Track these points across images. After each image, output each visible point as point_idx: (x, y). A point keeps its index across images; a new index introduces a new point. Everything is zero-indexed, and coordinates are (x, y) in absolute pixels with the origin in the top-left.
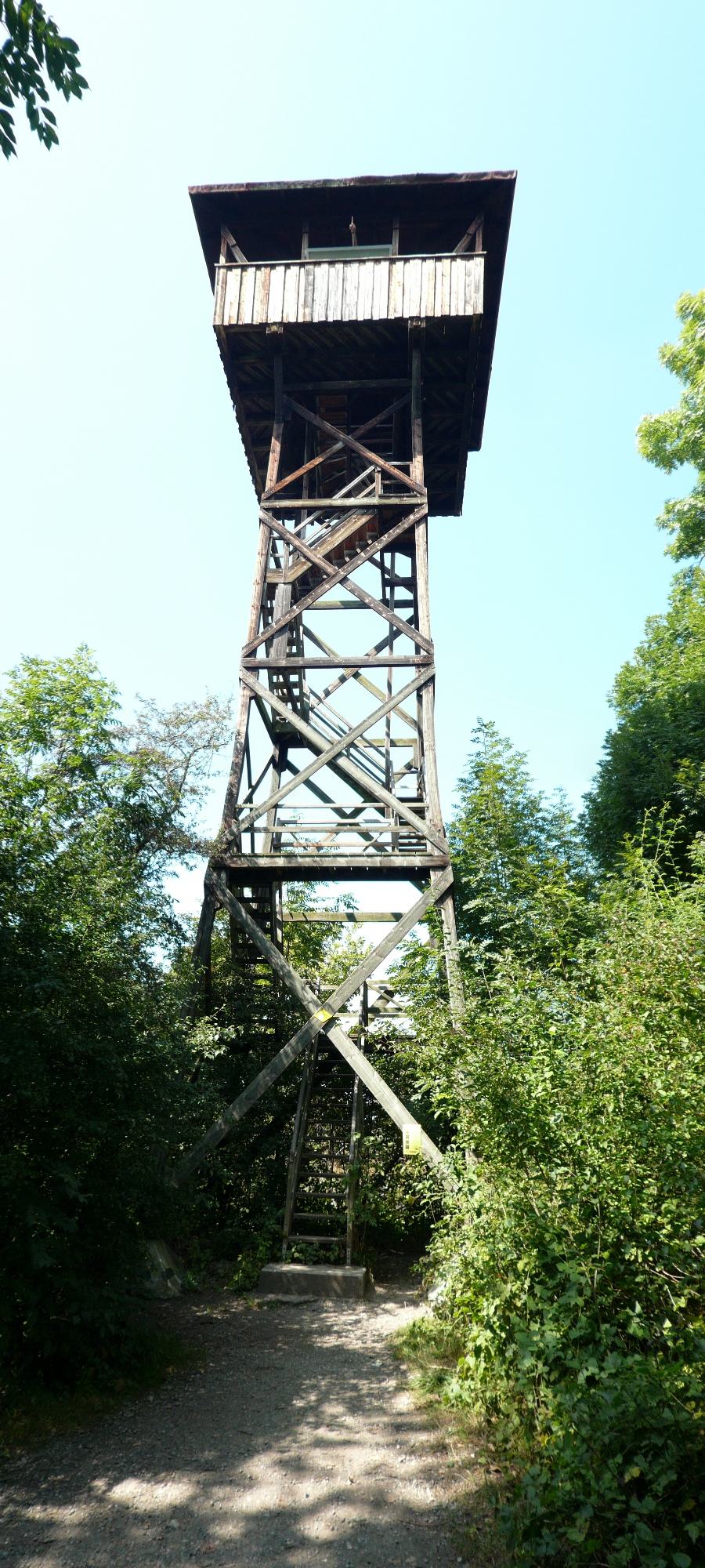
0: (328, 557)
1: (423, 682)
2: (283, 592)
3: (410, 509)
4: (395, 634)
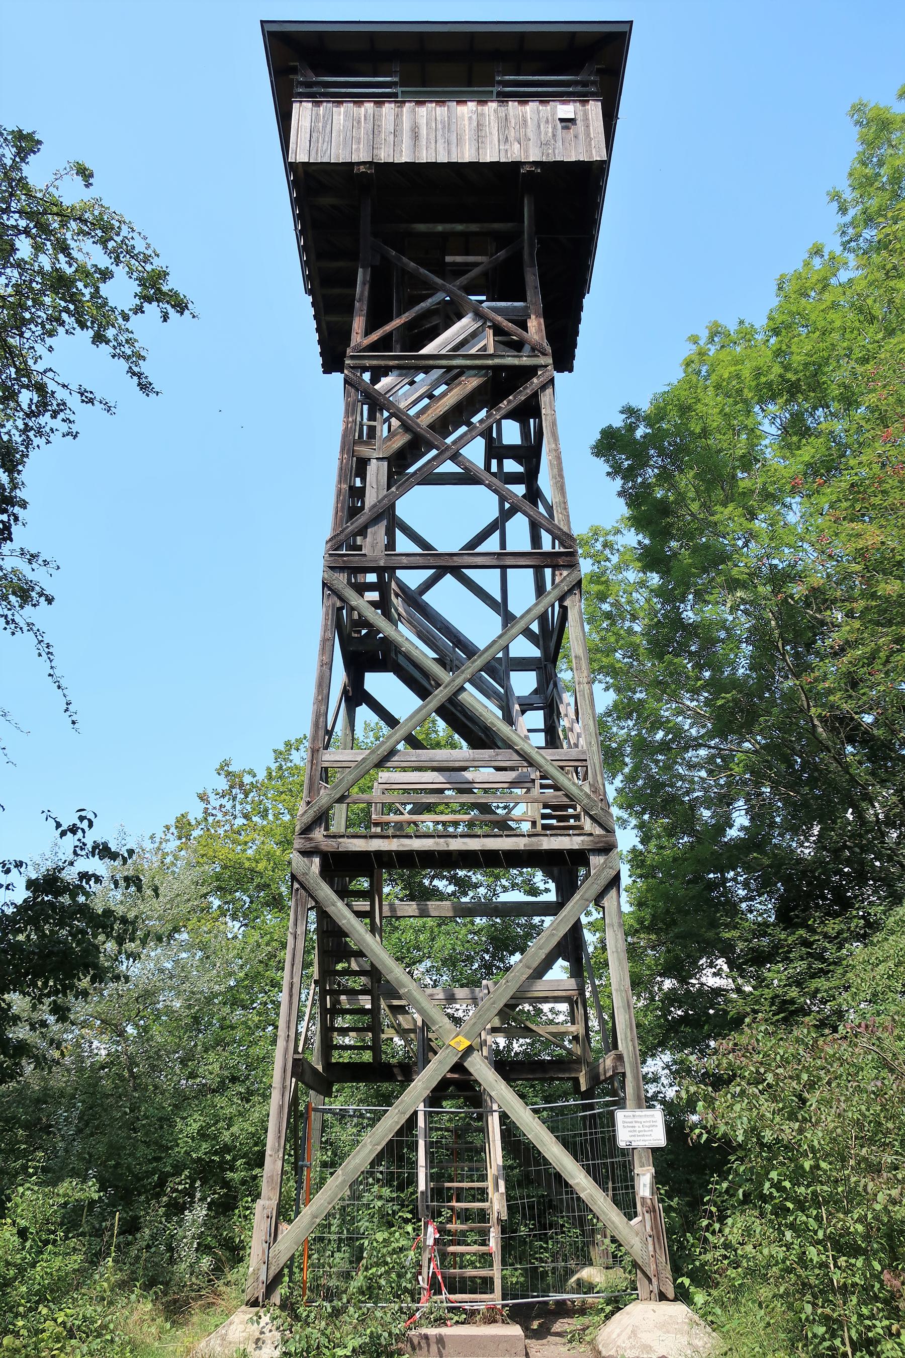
0: (431, 426)
1: (566, 588)
2: (377, 472)
3: (531, 371)
4: (505, 515)
